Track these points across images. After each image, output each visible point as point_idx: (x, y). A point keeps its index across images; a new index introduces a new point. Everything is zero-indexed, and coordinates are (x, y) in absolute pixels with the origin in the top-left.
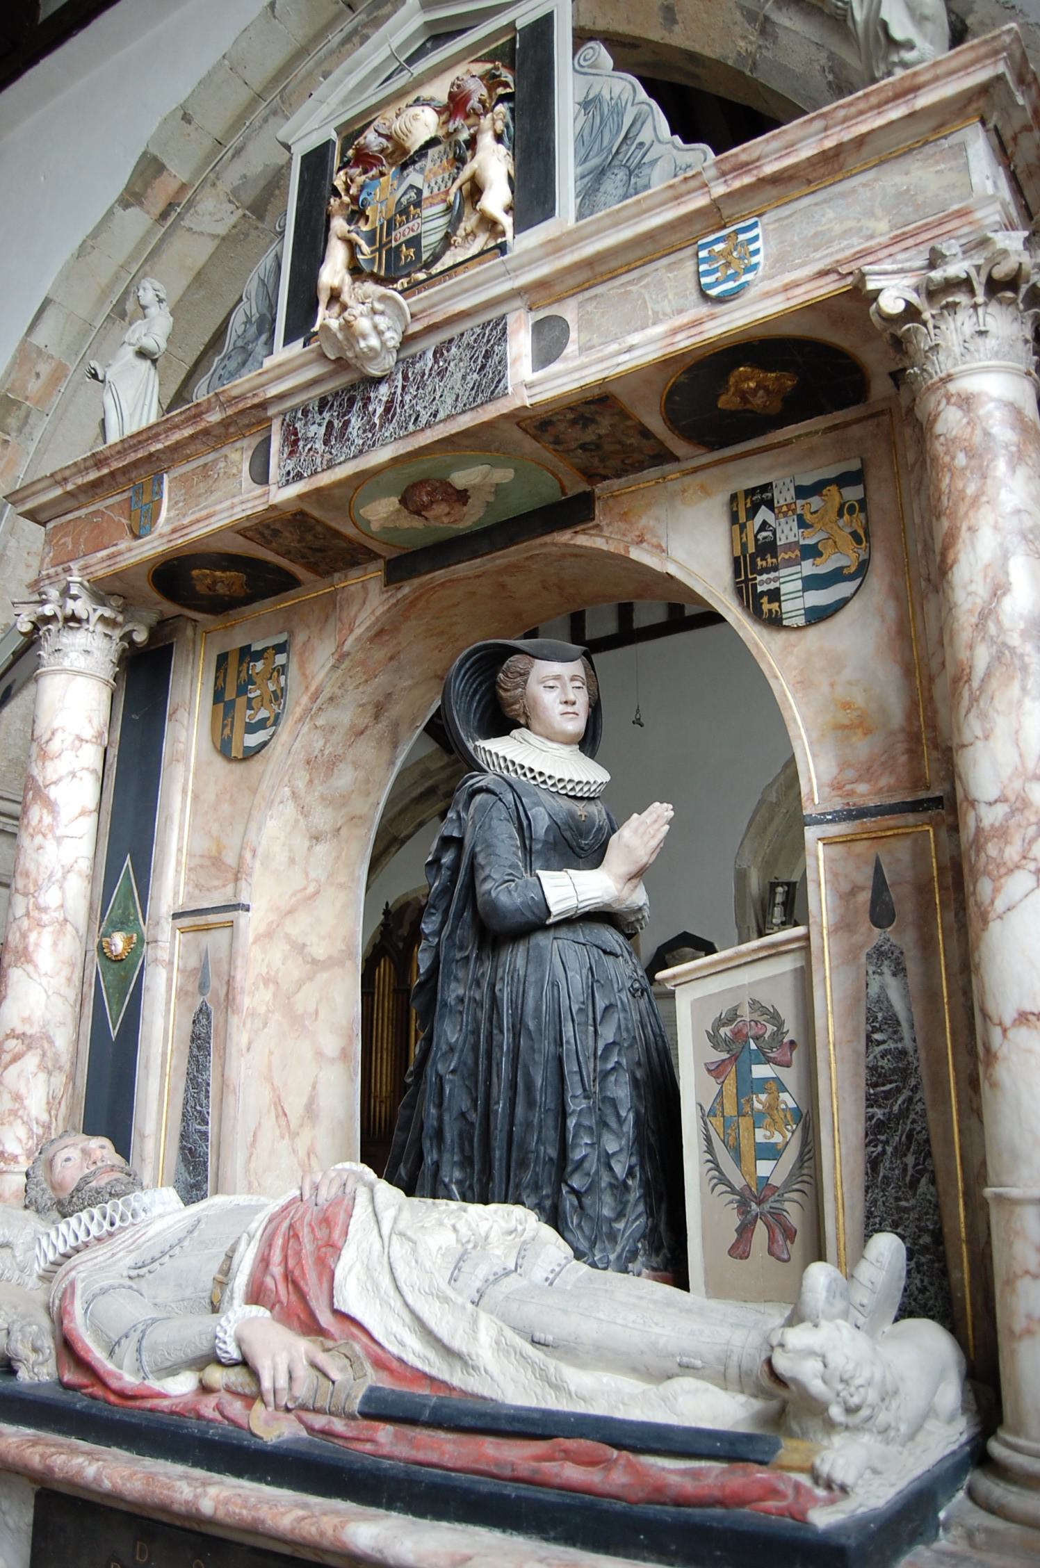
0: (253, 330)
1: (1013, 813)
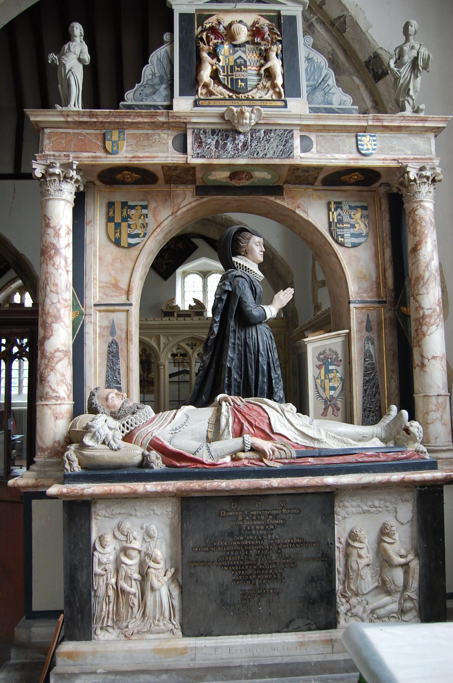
0: (157, 80)
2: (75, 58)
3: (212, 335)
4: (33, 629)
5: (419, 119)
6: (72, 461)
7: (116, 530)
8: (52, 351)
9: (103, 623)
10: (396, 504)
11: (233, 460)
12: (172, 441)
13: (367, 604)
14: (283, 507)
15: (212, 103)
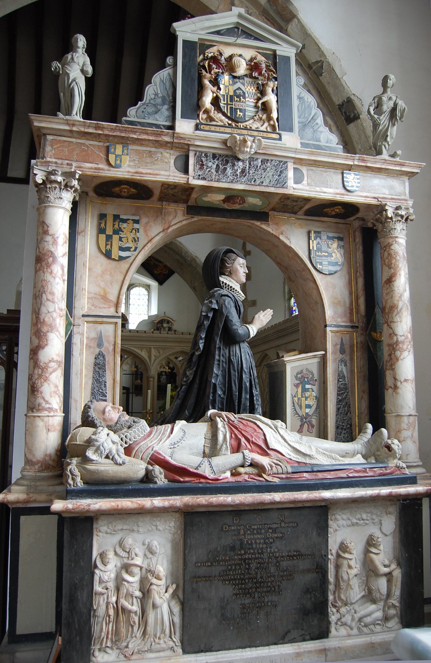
0: (159, 101)
1: (406, 338)
2: (78, 68)
3: (197, 350)
4: (18, 655)
5: (397, 163)
6: (76, 476)
7: (117, 546)
8: (47, 361)
9: (101, 644)
10: (381, 517)
11: (233, 475)
12: (173, 456)
13: (355, 613)
14: (282, 521)
15: (213, 128)
